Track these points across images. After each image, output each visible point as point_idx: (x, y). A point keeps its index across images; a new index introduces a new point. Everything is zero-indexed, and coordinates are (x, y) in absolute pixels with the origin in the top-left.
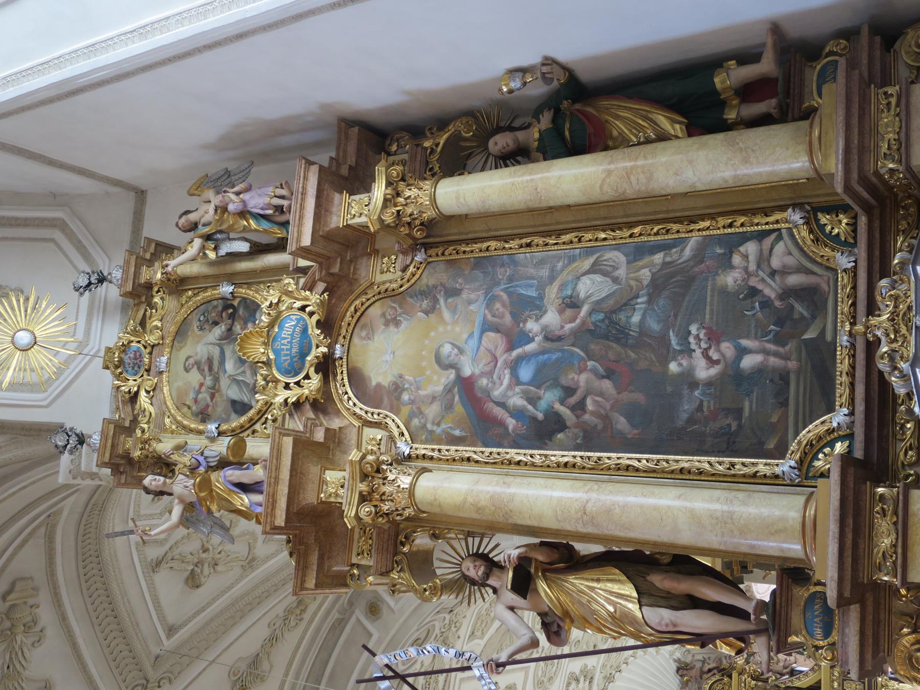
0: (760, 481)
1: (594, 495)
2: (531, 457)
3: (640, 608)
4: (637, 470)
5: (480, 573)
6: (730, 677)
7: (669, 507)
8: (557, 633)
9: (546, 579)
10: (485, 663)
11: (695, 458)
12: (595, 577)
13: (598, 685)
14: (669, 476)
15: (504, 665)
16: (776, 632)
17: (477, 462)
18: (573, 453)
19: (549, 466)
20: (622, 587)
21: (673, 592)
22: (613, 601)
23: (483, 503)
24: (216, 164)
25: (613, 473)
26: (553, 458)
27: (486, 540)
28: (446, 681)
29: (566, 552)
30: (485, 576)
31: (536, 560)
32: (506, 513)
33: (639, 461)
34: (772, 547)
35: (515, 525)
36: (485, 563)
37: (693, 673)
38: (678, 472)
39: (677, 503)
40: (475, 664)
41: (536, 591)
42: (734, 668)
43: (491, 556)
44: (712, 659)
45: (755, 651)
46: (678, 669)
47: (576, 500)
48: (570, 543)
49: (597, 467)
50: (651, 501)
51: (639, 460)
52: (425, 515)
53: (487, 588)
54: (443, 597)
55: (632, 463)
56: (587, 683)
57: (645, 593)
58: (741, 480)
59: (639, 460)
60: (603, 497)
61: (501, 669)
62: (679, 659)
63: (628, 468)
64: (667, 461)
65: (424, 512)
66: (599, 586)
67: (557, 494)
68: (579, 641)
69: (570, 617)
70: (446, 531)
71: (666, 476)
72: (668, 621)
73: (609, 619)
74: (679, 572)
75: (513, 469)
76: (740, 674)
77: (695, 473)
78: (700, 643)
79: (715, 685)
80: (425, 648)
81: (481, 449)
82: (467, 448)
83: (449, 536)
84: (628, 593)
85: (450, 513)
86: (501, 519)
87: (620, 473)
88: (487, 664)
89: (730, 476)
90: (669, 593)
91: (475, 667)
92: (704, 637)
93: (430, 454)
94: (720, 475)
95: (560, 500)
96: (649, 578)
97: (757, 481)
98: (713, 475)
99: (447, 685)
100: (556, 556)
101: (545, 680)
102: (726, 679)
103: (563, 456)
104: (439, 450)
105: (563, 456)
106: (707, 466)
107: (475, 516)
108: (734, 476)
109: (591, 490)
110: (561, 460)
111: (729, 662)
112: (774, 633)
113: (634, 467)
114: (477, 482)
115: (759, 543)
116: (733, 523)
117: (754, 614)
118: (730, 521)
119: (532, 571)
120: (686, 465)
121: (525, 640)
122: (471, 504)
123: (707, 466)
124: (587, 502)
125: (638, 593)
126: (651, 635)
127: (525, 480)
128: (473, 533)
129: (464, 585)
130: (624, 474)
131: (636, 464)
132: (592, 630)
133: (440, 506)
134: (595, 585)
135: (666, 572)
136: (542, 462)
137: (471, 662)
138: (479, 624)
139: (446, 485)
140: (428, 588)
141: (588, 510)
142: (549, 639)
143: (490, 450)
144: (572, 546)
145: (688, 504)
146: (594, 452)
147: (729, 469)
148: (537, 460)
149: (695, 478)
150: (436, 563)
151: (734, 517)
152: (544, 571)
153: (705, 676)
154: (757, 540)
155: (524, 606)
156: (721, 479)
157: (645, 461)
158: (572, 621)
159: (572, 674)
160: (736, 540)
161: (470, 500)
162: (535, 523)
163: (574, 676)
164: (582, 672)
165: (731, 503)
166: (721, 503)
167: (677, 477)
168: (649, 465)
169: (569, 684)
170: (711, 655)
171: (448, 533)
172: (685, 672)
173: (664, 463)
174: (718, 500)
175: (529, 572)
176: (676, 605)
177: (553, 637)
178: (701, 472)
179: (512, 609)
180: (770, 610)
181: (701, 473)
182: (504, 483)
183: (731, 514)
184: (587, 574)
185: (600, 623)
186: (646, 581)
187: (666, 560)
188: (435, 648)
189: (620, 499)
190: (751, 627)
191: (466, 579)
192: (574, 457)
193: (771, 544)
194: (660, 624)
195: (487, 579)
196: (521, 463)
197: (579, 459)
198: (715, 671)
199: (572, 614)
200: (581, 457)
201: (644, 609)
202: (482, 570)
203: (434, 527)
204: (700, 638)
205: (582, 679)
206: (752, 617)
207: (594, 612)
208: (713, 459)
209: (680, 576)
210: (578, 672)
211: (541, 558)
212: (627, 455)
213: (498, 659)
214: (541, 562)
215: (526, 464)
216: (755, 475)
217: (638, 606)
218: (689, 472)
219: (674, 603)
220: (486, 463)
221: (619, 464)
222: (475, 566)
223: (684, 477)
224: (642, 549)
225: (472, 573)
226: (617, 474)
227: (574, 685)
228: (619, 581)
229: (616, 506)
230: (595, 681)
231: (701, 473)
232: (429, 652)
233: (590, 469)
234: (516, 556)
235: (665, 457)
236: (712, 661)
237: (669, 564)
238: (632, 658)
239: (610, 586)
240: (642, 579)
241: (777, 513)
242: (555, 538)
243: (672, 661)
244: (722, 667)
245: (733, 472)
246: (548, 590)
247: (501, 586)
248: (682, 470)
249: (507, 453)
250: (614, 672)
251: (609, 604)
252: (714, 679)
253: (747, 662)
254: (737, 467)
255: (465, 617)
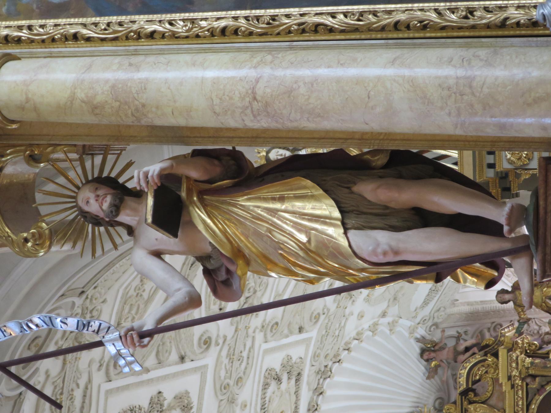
0: (512, 33)
1: (267, 71)
2: (171, 24)
3: (345, 233)
4: (331, 30)
5: (106, 206)
6: (496, 355)
7: (379, 78)
8: (227, 283)
9: (205, 206)
10: (122, 334)
11: (416, 5)
12: (277, 195)
13: (308, 384)
14: (379, 36)
15: (150, 334)
16: (540, 248)
17: (88, 39)
18: (233, 13)
19: (198, 36)
20: (318, 204)
21: (392, 205)
22: (305, 226)
23: (100, 98)
24: (22, 397)
25: (296, 39)
26: (203, 23)
27: (111, 158)
28: (85, 396)
29: (232, 162)
30: (113, 209)
31: (188, 178)
32: (137, 110)
33: (334, 17)
34: (530, 125)
35: (153, 128)
36: (112, 191)
37: (444, 355)
38: (391, 28)
39: (390, 72)
40: (107, 337)
41: (191, 224)
42: (501, 343)
43: (121, 180)
44: (470, 333)
45: (529, 317)
46: (423, 352)
47: (241, 80)
48: (238, 148)
49: (270, 31)
50: (352, 72)
51: (333, 15)
52: (14, 126)
53: (120, 229)
54: (54, 249)
55: (322, 21)
56: (293, 381)
57: (352, 211)
58: (483, 33)
59: (333, 15)
60: (280, 73)
61: (146, 340)
62: (423, 337)
63: (317, 28)
64: (375, 13)
65: (13, 122)
66: (283, 207)
67: (210, 74)
68: (277, 324)
69: (244, 257)
70: (50, 149)
71: (373, 36)
72: (386, 247)
73: (301, 253)
74: (400, 176)
75: (145, 45)
76: (510, 350)
77: (417, 29)
78: (434, 274)
79: (476, 369)
80: (31, 321)
81: (93, 19)
82: (72, 20)
83: (55, 156)
84: (326, 213)
85: (53, 118)
86: (129, 121)
87: (306, 36)
88: (126, 335)
89: (467, 28)
90: (386, 207)
91: (107, 341)
92: (439, 266)
93: (16, 34)
94: (453, 28)
95: (216, 81)
96: (356, 189)
97: (506, 33)
98: (443, 28)
99: (87, 401)
100: (216, 169)
101: (231, 383)
102: (490, 359)
103: (218, 19)
104: (30, 28)
105: (218, 19)
106: (433, 16)
107: (90, 119)
108: (473, 27)
109: (262, 63)
110: (216, 24)
111: (494, 334)
112: (537, 249)
113: (326, 25)
114: (89, 68)
115: (511, 120)
116: (473, 94)
117: (508, 224)
118: (468, 91)
119: (183, 194)
120: (402, 17)
121: (179, 297)
122: (83, 101)
123: (433, 16)
124: (257, 81)
125: (341, 212)
126: (363, 270)
127: (162, 59)
128: (91, 147)
129: (83, 225)
130: (312, 38)
131: (329, 21)
132: (278, 273)
133: (35, 109)
134: (277, 206)
135: (381, 177)
136: (187, 31)
137: (101, 334)
138: (126, 310)
139: (42, 76)
140: (29, 237)
141: (259, 93)
142: (215, 291)
143: (106, 19)
144: (241, 153)
145: (406, 72)
146: (266, 8)
147: (466, 17)
148: (180, 28)
149: (417, 35)
150: (39, 197)
151: (474, 84)
152: (201, 194)
153: (461, 358)
154: (508, 115)
155: (176, 249)
156: (455, 34)
157: (341, 17)
158: (248, 263)
159: (270, 371)
160: (477, 119)
161: (81, 95)
162: (181, 122)
163: (273, 373)
164: (283, 366)
165: (469, 64)
166: (455, 66)
167: (390, 36)
168: (348, 21)
169: (266, 386)
170: (468, 328)
171: (53, 152)
172: (433, 355)
173: (370, 16)
174: (450, 61)
175: (179, 198)
176: (397, 224)
177: (221, 288)
178: (425, 26)
179: (158, 254)
180: (531, 218)
181: (425, 27)
182: (130, 65)
183: (470, 81)
184: (266, 191)
185: (289, 261)
186: (352, 193)
187: (381, 160)
188: (47, 320)
189: (306, 72)
190: (506, 245)
191: (85, 217)
192: (236, 18)
193: (528, 120)
194: (374, 252)
195: (117, 215)
196: (155, 35)
197: (243, 21)
198: (475, 350)
199: (246, 252)
200: (247, 18)
201: (352, 233)
202: (108, 201)
203: (31, 145)
204: (435, 267)
205: (285, 377)
206: (506, 229)
207: (279, 245)
208: (441, 5)
209: (400, 182)
210: (278, 367)
211: (194, 174)
212: (315, 9)
213: (142, 327)
214: (196, 181)
215: (163, 36)
216: (503, 24)
217: (342, 231)
218: (408, 27)
219: (394, 221)
220: (103, 40)
221: (303, 24)
222: (98, 196)
223: (401, 36)
224: (343, 147)
225: (94, 208)
226: (301, 38)
227: (273, 385)
228: (313, 197)
229: (301, 84)
230: (305, 378)
231: (425, 27)
232: (37, 326)
233: (261, 35)
234: (156, 172)
235: (371, 7)
236: (470, 336)
237: (385, 167)
238: (356, 342)
239: (298, 205)
240: (347, 190)
241: (535, 73)
242: (213, 143)
243: (413, 341)
244: (484, 343)
245: (471, 22)
246: (209, 221)
247: (139, 223)
248: (396, 25)
249: (134, 22)
250: (330, 364)
251: (300, 231)
252: (473, 361)
253: (519, 333)
254: (478, 14)
255: (104, 302)
